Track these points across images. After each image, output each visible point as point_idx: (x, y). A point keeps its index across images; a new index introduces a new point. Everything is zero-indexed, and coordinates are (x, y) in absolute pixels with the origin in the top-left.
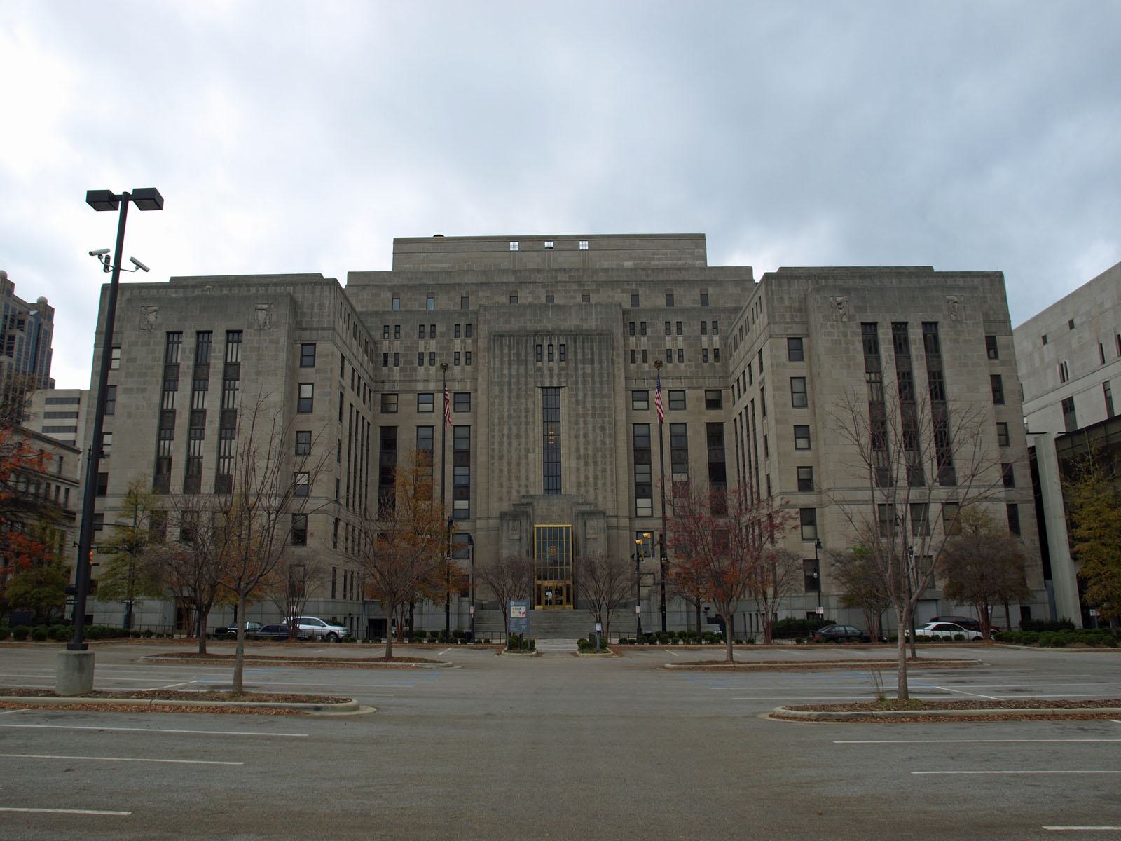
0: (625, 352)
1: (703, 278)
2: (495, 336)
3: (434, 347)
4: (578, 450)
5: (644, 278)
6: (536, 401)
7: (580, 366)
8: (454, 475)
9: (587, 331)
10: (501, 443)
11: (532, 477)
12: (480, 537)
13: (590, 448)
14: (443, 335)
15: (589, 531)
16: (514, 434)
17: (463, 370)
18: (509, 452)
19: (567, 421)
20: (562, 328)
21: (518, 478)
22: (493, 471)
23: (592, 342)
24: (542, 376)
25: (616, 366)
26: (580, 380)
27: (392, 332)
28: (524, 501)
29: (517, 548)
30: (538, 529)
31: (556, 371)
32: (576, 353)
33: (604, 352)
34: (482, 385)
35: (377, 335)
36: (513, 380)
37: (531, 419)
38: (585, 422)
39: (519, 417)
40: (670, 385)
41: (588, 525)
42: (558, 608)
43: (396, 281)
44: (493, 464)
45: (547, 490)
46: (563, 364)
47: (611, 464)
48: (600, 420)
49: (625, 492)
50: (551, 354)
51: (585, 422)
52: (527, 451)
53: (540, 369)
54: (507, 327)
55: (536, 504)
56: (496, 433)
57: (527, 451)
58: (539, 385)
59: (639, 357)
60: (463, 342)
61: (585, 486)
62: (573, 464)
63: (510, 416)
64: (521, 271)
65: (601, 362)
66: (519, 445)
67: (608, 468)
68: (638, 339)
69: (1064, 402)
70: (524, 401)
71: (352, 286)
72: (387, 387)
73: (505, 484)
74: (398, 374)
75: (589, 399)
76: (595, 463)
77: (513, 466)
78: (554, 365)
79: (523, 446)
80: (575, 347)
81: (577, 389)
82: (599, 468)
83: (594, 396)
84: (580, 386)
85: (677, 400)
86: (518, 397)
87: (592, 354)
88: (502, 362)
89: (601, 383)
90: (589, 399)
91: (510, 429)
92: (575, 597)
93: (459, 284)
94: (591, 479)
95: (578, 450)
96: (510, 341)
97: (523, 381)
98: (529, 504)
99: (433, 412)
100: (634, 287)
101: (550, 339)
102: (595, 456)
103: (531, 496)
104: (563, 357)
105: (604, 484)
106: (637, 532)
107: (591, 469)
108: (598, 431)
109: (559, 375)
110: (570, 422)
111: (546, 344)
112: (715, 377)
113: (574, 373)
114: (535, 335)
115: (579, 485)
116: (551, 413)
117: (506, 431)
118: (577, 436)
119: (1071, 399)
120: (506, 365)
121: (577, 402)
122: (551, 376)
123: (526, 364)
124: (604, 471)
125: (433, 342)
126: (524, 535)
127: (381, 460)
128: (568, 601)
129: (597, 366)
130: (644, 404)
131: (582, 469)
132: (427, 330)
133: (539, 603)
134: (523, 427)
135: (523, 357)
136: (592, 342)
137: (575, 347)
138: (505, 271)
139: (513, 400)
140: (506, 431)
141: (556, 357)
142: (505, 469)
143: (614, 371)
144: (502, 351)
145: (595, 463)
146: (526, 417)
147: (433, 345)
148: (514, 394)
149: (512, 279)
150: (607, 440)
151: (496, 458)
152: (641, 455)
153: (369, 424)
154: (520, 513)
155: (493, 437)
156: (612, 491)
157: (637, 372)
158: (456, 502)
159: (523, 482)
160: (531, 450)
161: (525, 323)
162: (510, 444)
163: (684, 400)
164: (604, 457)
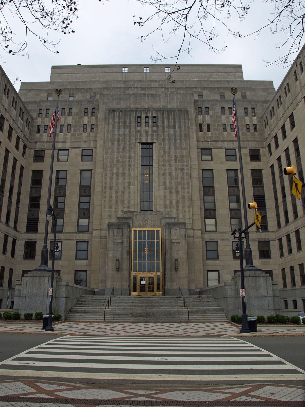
0: (196, 125)
1: (242, 86)
2: (109, 111)
3: (71, 121)
4: (165, 183)
5: (206, 86)
6: (136, 152)
7: (166, 129)
8: (79, 203)
9: (171, 108)
10: (111, 179)
11: (132, 202)
12: (95, 243)
13: (174, 182)
14: (77, 114)
15: (173, 237)
16: (120, 173)
17: (89, 135)
18: (117, 184)
19: (157, 164)
20: (154, 107)
21: (123, 202)
22: (105, 197)
23: (174, 115)
24: (141, 135)
25: (190, 130)
26: (166, 138)
27: (44, 112)
28: (126, 215)
29: (120, 249)
30: (135, 231)
31: (150, 133)
32: (163, 122)
33: (182, 121)
34: (100, 141)
35: (34, 115)
36: (121, 138)
37: (132, 163)
38: (170, 165)
39: (125, 162)
40: (226, 146)
41: (173, 233)
42: (150, 294)
43: (51, 87)
44: (105, 192)
45: (143, 210)
46: (155, 128)
47: (188, 193)
48: (179, 164)
49: (198, 213)
50: (147, 123)
51: (170, 165)
52: (130, 184)
53: (139, 131)
54: (118, 107)
55: (134, 218)
56: (109, 172)
57: (130, 184)
58: (138, 141)
59: (205, 128)
60: (90, 118)
61: (170, 208)
62: (162, 192)
63: (118, 161)
64: (128, 81)
65: (180, 127)
66: (124, 179)
67: (186, 195)
68: (204, 118)
69: (290, 267)
70: (128, 151)
71: (23, 90)
72: (38, 146)
73: (113, 206)
74: (46, 138)
75: (172, 150)
76: (177, 192)
77: (120, 194)
78: (149, 129)
79: (127, 180)
80: (163, 118)
81: (164, 144)
82: (180, 195)
83: (176, 148)
84: (166, 142)
85: (231, 154)
86: (124, 148)
87: (174, 122)
88: (114, 126)
89: (181, 140)
90: (172, 150)
91: (118, 169)
92: (164, 286)
93: (90, 89)
94: (174, 203)
95: (165, 183)
96: (119, 114)
97: (127, 138)
98: (130, 218)
99: (68, 161)
100: (200, 90)
101: (146, 113)
102: (177, 188)
103: (131, 212)
104: (155, 124)
105: (183, 207)
106: (206, 242)
107: (174, 196)
108: (179, 172)
109: (152, 135)
110: (159, 165)
111: (143, 116)
112: (255, 141)
113: (162, 134)
114: (137, 110)
115: (166, 207)
116: (147, 158)
117: (115, 171)
118: (164, 174)
119: (293, 267)
120: (116, 129)
121: (164, 152)
122: (147, 135)
123: (130, 128)
124: (183, 197)
125: (70, 118)
126: (125, 240)
127: (31, 191)
128: (158, 288)
129: (178, 129)
130: (209, 157)
131: (168, 196)
132: (67, 111)
133: (135, 290)
134: (127, 168)
135: (128, 124)
136: (174, 115)
137: (163, 118)
138: (119, 81)
139: (120, 150)
140: (115, 171)
141: (150, 124)
142: (114, 196)
143: (189, 134)
144: (114, 120)
145: (177, 192)
146: (129, 161)
147: (70, 120)
148: (121, 147)
149: (123, 86)
150: (185, 177)
151: (108, 188)
152: (208, 189)
153: (22, 168)
154: (122, 224)
155: (106, 174)
156: (189, 211)
157: (204, 137)
158: (80, 220)
159: (126, 205)
160: (132, 183)
161: (130, 104)
162: (117, 179)
163: (214, 202)
164: (183, 188)
